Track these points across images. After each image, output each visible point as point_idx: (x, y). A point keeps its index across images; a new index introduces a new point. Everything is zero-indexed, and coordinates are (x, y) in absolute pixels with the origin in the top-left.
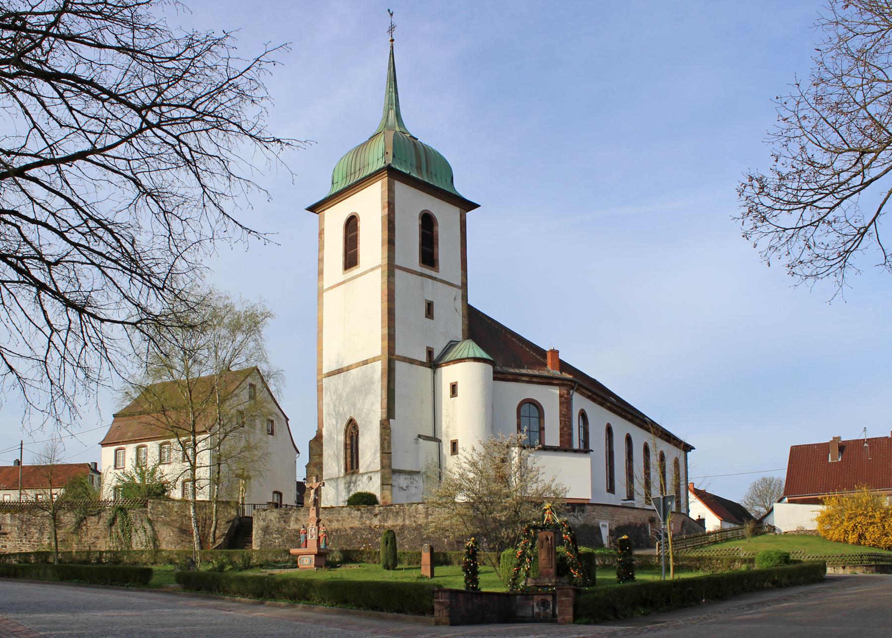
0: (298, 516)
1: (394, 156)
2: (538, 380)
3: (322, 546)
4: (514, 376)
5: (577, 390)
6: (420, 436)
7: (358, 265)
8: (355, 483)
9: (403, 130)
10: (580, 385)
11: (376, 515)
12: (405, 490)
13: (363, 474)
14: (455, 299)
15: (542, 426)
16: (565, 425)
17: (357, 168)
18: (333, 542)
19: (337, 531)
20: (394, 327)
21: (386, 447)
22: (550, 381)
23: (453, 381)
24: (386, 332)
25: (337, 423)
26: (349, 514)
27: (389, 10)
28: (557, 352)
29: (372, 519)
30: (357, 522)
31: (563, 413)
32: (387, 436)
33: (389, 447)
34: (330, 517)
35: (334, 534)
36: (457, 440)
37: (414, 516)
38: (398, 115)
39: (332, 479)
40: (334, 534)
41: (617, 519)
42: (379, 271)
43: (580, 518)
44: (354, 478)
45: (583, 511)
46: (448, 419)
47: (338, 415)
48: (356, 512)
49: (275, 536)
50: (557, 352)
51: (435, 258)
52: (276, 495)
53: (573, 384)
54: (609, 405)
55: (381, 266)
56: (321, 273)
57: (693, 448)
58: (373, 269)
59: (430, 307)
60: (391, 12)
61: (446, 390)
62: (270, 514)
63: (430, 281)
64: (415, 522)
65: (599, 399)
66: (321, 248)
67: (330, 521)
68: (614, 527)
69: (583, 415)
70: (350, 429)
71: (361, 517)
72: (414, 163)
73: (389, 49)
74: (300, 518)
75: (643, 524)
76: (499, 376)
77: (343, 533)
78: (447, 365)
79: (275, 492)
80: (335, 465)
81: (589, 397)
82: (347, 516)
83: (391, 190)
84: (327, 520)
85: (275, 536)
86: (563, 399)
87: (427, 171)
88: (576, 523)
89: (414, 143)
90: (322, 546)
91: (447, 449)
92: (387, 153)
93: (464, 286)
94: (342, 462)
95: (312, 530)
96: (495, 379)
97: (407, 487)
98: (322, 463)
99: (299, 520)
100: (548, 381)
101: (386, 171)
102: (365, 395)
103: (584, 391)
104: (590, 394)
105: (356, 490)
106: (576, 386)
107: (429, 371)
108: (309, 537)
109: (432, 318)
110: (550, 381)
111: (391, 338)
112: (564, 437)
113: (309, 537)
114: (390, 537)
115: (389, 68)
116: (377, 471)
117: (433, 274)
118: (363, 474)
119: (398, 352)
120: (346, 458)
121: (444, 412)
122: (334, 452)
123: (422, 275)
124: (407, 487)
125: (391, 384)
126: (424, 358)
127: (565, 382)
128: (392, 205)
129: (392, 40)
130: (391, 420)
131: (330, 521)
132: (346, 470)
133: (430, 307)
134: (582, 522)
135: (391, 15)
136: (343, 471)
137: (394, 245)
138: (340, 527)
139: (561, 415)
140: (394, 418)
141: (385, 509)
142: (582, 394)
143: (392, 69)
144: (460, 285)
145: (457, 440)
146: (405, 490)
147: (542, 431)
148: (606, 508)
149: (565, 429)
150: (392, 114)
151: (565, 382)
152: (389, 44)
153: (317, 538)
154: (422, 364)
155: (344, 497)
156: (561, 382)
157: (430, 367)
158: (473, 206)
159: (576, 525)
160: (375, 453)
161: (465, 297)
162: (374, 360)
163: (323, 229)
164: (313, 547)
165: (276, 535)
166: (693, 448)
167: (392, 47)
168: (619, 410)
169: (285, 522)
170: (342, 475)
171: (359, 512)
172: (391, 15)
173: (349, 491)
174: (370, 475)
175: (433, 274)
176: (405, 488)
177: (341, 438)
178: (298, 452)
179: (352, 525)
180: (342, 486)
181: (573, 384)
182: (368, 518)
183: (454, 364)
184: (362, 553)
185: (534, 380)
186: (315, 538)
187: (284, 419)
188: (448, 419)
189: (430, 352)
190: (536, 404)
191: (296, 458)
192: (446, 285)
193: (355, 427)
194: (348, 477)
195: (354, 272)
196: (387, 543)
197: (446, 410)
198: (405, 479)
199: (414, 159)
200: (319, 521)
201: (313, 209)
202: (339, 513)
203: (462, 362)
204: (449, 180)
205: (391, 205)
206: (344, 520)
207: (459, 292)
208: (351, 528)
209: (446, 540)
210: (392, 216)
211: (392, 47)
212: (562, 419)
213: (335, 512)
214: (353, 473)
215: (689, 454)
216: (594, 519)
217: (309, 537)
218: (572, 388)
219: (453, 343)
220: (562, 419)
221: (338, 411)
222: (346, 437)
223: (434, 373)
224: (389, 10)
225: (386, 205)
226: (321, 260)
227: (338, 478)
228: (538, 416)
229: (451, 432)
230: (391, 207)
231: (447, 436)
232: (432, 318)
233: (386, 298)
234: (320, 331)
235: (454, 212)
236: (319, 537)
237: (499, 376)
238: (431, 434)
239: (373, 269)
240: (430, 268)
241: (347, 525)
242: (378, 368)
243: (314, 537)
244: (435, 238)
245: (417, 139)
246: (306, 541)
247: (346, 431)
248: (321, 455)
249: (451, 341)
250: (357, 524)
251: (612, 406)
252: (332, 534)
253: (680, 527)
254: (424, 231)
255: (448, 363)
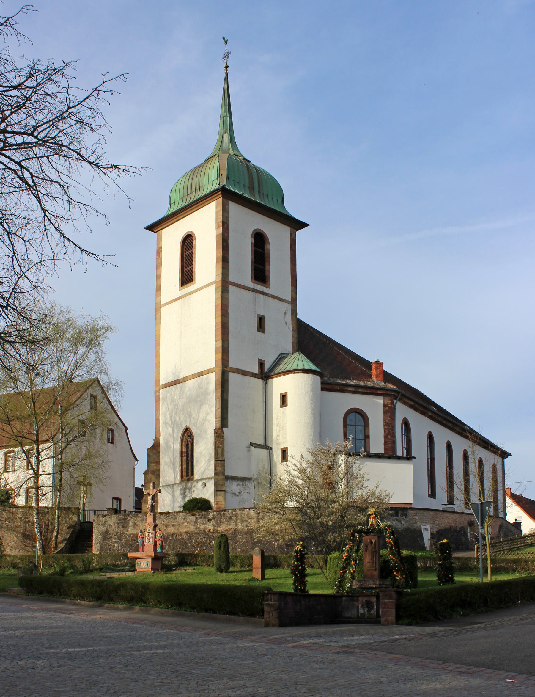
0: (136, 521)
1: (228, 178)
2: (363, 391)
3: (159, 550)
4: (341, 387)
5: (400, 400)
6: (251, 444)
7: (194, 282)
8: (190, 489)
9: (236, 153)
10: (403, 395)
11: (210, 520)
12: (238, 496)
13: (198, 481)
14: (285, 313)
15: (367, 434)
16: (389, 434)
17: (194, 189)
18: (169, 546)
19: (173, 535)
20: (227, 340)
21: (220, 455)
22: (374, 391)
23: (283, 391)
24: (220, 345)
25: (173, 432)
26: (184, 519)
27: (224, 38)
28: (382, 364)
29: (206, 523)
30: (192, 527)
31: (387, 421)
32: (221, 444)
33: (223, 455)
34: (166, 522)
35: (170, 538)
36: (287, 448)
37: (246, 521)
38: (232, 139)
39: (169, 485)
40: (170, 538)
41: (438, 522)
42: (214, 287)
43: (403, 522)
44: (189, 485)
45: (406, 515)
46: (278, 428)
47: (175, 424)
48: (191, 517)
49: (114, 540)
50: (382, 364)
51: (266, 274)
52: (115, 501)
53: (396, 394)
54: (430, 414)
55: (215, 282)
56: (158, 289)
57: (510, 455)
58: (208, 285)
59: (261, 320)
60: (226, 39)
61: (276, 400)
62: (109, 519)
63: (262, 296)
64: (247, 526)
65: (421, 409)
66: (159, 265)
67: (167, 526)
68: (435, 531)
69: (406, 423)
70: (186, 438)
71: (196, 522)
72: (247, 185)
73: (224, 76)
74: (138, 523)
75: (463, 527)
76: (327, 387)
77: (179, 537)
78: (277, 377)
79: (114, 498)
80: (171, 471)
81: (411, 407)
82: (182, 521)
83: (225, 210)
84: (164, 524)
85: (114, 540)
86: (387, 408)
87: (259, 192)
88: (400, 526)
89: (247, 165)
90: (159, 550)
91: (277, 456)
92: (222, 175)
93: (294, 301)
94: (178, 469)
95: (149, 535)
96: (322, 389)
97: (239, 493)
98: (159, 471)
99: (137, 525)
100: (373, 391)
101: (221, 192)
102: (200, 406)
103: (407, 400)
104: (412, 403)
105: (191, 496)
106: (399, 397)
107: (260, 382)
108: (146, 541)
109: (263, 332)
110: (374, 391)
111: (225, 351)
112: (388, 445)
113: (147, 541)
114: (223, 541)
115: (224, 94)
116: (211, 478)
117: (265, 290)
118: (198, 481)
119: (232, 364)
120: (182, 465)
121: (274, 421)
122: (171, 459)
123: (254, 290)
124: (239, 493)
125: (225, 395)
126: (255, 370)
127: (389, 392)
128: (226, 225)
129: (227, 67)
130: (224, 429)
131: (167, 526)
132: (182, 476)
133: (261, 320)
134: (405, 526)
135: (226, 42)
136: (179, 477)
137: (228, 262)
138: (176, 531)
139: (386, 424)
140: (227, 427)
141: (219, 514)
142: (405, 403)
143: (226, 95)
144: (290, 300)
145: (287, 448)
146: (238, 496)
147: (367, 439)
148: (428, 512)
149: (389, 437)
150: (226, 137)
151: (389, 392)
152: (224, 70)
153: (154, 543)
154: (254, 375)
155: (180, 502)
156: (385, 392)
157: (262, 378)
158: (302, 225)
159: (400, 528)
160: (209, 460)
161: (294, 312)
162: (209, 371)
163: (161, 248)
164: (150, 551)
165: (115, 539)
166: (510, 455)
167: (227, 73)
168: (440, 419)
169: (124, 527)
170: (178, 482)
171: (194, 517)
172: (226, 42)
173: (185, 497)
174: (204, 481)
175: (265, 290)
176: (237, 494)
177: (177, 446)
178: (137, 460)
179: (187, 530)
180: (178, 492)
181: (396, 394)
182: (202, 523)
183: (284, 375)
184: (196, 556)
185: (360, 390)
186: (152, 542)
187: (124, 428)
188: (278, 428)
189: (261, 364)
190: (357, 411)
191: (134, 465)
192: (277, 300)
193: (191, 435)
194: (184, 484)
195: (190, 288)
196: (220, 547)
197: (277, 419)
198: (238, 485)
199: (247, 181)
200: (155, 526)
201: (151, 228)
202: (175, 519)
203: (291, 373)
204: (280, 201)
205: (225, 225)
206: (179, 525)
207: (289, 307)
208: (187, 533)
209: (276, 543)
210: (226, 234)
211: (227, 73)
212: (386, 427)
213: (171, 517)
214: (188, 480)
215: (506, 460)
216: (416, 522)
217: (147, 541)
218: (396, 398)
219: (283, 356)
220: (386, 427)
221: (175, 421)
222: (182, 446)
223: (266, 384)
224: (224, 38)
225: (221, 224)
226: (159, 277)
227: (174, 485)
228: (363, 424)
229: (281, 440)
230: (225, 226)
231: (278, 444)
232: (263, 332)
233: (220, 313)
234: (158, 344)
235: (285, 230)
236: (156, 542)
237: (327, 387)
238: (262, 442)
239: (208, 285)
240: (262, 284)
241: (183, 529)
242: (213, 379)
243: (151, 541)
244: (266, 255)
245: (250, 162)
246: (144, 545)
247: (182, 440)
248: (158, 463)
249: (282, 354)
250: (191, 528)
251: (433, 415)
252: (168, 538)
253: (497, 530)
254: (256, 248)
255: (279, 374)
